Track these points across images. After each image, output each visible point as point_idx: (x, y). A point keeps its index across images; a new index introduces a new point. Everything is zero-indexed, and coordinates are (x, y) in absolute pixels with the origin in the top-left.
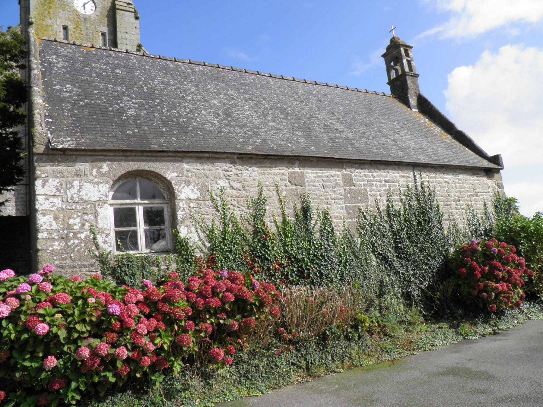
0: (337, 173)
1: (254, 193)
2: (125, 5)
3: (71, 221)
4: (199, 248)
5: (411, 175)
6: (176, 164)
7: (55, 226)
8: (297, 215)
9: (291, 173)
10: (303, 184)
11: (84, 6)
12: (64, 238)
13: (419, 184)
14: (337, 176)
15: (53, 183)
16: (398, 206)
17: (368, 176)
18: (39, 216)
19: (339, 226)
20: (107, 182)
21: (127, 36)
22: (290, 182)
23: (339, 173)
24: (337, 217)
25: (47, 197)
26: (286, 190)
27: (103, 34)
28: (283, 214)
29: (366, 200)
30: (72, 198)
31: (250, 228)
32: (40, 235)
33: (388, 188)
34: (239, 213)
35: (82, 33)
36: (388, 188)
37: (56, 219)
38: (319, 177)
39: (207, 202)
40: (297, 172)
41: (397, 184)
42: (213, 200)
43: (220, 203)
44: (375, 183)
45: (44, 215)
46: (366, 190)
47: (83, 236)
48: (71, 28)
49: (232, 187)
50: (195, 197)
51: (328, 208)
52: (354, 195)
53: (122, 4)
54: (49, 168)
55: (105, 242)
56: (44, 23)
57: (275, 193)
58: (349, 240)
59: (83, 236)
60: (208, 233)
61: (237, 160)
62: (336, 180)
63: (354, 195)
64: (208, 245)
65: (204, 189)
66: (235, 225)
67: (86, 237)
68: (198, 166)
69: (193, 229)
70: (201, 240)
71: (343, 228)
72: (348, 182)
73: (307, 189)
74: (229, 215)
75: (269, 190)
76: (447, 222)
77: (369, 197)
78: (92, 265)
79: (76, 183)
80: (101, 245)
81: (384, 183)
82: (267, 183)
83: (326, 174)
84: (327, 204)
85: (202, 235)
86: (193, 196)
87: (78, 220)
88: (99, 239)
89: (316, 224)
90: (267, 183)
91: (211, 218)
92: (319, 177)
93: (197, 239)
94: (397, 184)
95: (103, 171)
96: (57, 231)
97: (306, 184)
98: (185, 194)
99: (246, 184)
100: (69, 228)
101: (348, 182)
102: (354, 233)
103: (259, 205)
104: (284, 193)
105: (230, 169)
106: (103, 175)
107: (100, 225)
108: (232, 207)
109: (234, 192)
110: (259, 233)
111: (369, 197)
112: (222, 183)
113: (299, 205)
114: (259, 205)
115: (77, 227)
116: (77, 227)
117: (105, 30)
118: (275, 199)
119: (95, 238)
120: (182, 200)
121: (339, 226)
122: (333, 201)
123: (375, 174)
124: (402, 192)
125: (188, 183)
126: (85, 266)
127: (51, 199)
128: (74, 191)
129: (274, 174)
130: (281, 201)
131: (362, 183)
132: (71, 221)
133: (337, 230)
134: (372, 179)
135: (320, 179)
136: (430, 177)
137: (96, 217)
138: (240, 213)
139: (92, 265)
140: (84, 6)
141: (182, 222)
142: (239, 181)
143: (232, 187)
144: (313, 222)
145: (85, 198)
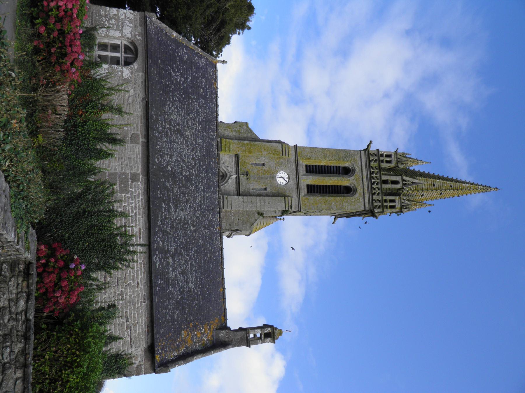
0: (140, 170)
1: (125, 109)
2: (290, 204)
3: (113, 20)
4: (96, 73)
5: (142, 242)
6: (141, 69)
7: (111, 13)
8: (111, 134)
9: (139, 135)
10: (132, 142)
11: (282, 177)
12: (106, 16)
13: (135, 249)
14: (138, 170)
15: (132, 17)
16: (118, 222)
17: (139, 196)
18: (117, 9)
19: (103, 164)
20: (132, 37)
21: (267, 204)
22: (133, 134)
23: (139, 172)
24: (109, 163)
25: (125, 14)
26: (128, 130)
27: (265, 189)
28: (113, 125)
29: (122, 192)
30: (124, 22)
31: (105, 103)
32: (108, 8)
33: (131, 214)
34: (115, 98)
35: (263, 175)
36: (131, 214)
37: (115, 15)
38: (137, 156)
39: (121, 81)
40: (139, 140)
41: (134, 225)
42: (122, 85)
43: (120, 88)
44: (134, 201)
45: (117, 11)
46: (128, 193)
47: (106, 23)
48: (264, 168)
49: (129, 97)
50: (124, 76)
51: (116, 158)
52: (126, 180)
53: (290, 202)
54: (138, 17)
55: (103, 31)
56: (263, 150)
57: (126, 122)
58: (92, 171)
59: (106, 23)
60: (104, 79)
61: (145, 101)
62: (135, 167)
63: (126, 180)
64: (98, 77)
65: (127, 81)
66: (107, 95)
67: (106, 25)
68: (141, 80)
69: (107, 71)
70: (101, 74)
71: (102, 167)
72: (134, 178)
73: (129, 145)
74: (113, 92)
75: (128, 119)
76: (103, 279)
77: (124, 195)
78: (92, 24)
79: (131, 25)
80: (102, 30)
81: (134, 212)
82: (132, 119)
83: (139, 161)
84: (119, 158)
85: (103, 76)
86: (124, 75)
87: (114, 23)
88: (104, 29)
89: (105, 146)
90: (132, 119)
91: (113, 82)
92: (137, 156)
93: (101, 73)
94: (134, 225)
95: (137, 37)
96: (109, 14)
97: (132, 145)
98: (126, 72)
99: (131, 105)
100: (111, 19)
101: (134, 178)
102: (99, 176)
103: (119, 111)
104: (126, 129)
105: (140, 97)
106: (135, 36)
107: (111, 31)
108: (118, 95)
109: (127, 98)
110: (103, 109)
111: (124, 195)
112: (132, 92)
113: (118, 137)
114: (119, 111)
115: (111, 22)
116: (111, 22)
117: (269, 190)
118: (123, 123)
119: (105, 28)
120: (122, 68)
121: (103, 164)
122: (120, 163)
123: (140, 204)
124: (128, 228)
125: (131, 73)
126: (92, 21)
127: (124, 15)
128: (128, 24)
129: (138, 124)
130: (120, 125)
131: (134, 190)
132: (113, 20)
133: (100, 163)
134: (137, 200)
135: (135, 156)
136: (141, 263)
137: (115, 30)
138: (115, 99)
139: (92, 24)
140: (282, 177)
141: (111, 67)
142: (133, 101)
143: (129, 97)
144: (107, 145)
145: (124, 27)
